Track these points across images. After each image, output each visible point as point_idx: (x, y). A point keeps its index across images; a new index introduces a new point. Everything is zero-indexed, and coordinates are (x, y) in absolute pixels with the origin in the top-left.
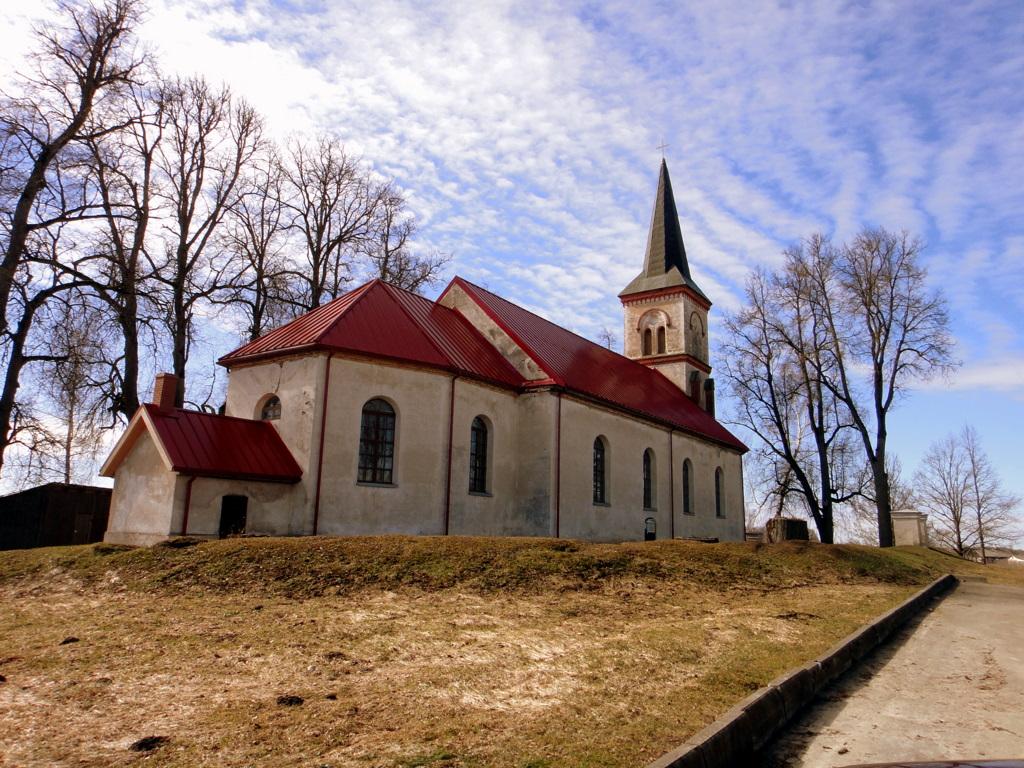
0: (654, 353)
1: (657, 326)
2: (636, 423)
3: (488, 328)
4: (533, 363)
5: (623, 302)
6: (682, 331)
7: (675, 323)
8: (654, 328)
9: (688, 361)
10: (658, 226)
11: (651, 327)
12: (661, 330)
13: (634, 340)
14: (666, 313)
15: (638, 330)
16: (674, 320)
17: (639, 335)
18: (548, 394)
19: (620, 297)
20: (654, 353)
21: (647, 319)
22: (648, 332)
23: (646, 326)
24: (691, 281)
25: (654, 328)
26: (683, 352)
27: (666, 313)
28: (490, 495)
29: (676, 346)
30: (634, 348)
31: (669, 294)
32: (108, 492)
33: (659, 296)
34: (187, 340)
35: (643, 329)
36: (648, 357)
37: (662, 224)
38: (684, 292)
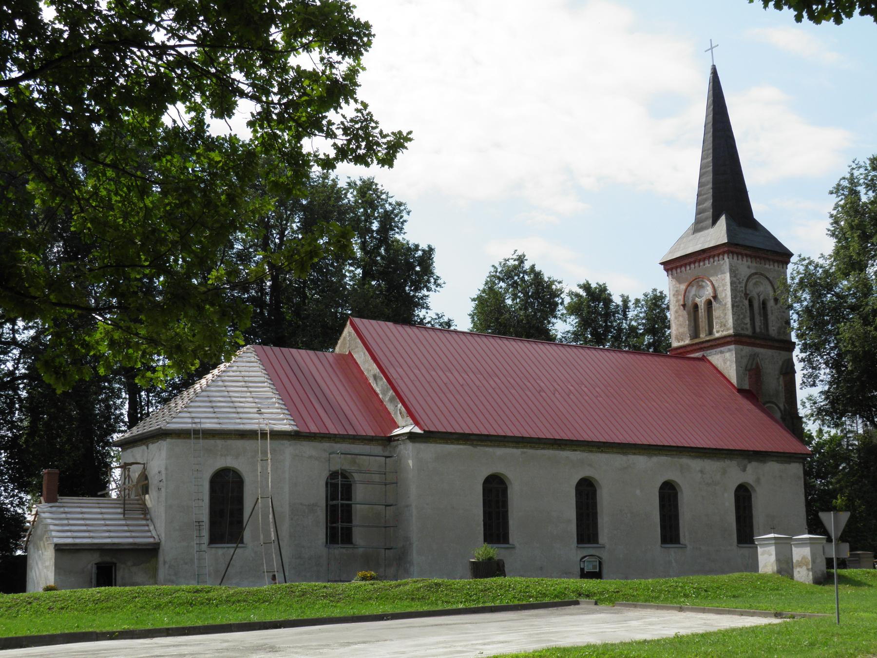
0: (703, 336)
1: (704, 299)
2: (562, 453)
3: (372, 372)
4: (403, 409)
5: (667, 270)
6: (729, 305)
7: (720, 296)
8: (701, 302)
9: (736, 342)
10: (705, 161)
11: (697, 300)
12: (709, 304)
13: (681, 319)
14: (712, 284)
15: (684, 306)
16: (719, 290)
17: (685, 313)
18: (408, 441)
19: (661, 264)
20: (703, 336)
21: (693, 291)
22: (696, 306)
23: (694, 300)
24: (755, 225)
25: (701, 302)
26: (731, 332)
27: (712, 284)
28: (685, 547)
29: (723, 325)
30: (681, 330)
31: (714, 257)
32: (106, 495)
33: (685, 265)
34: (51, 656)
35: (690, 303)
36: (697, 341)
37: (710, 159)
38: (728, 252)
